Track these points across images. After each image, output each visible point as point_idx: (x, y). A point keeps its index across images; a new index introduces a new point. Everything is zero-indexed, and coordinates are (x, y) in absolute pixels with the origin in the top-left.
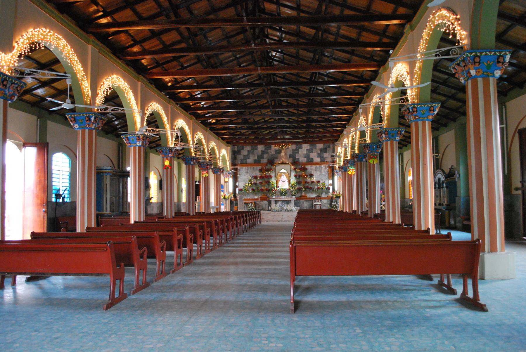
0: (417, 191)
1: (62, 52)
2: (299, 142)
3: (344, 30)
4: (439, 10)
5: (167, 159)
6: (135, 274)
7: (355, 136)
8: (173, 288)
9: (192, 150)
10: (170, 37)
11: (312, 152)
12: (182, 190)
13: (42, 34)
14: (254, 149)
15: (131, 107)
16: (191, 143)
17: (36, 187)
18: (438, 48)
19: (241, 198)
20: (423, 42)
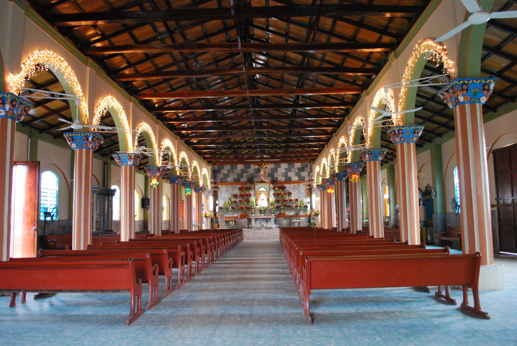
0: (404, 209)
1: (63, 74)
2: (278, 162)
3: (329, 56)
4: (424, 40)
5: (154, 177)
6: (149, 291)
7: (334, 156)
8: (185, 304)
9: (177, 169)
10: (160, 61)
11: (290, 171)
12: (163, 209)
13: (46, 57)
14: (233, 168)
15: (123, 128)
16: (176, 162)
17: (27, 205)
18: (421, 77)
19: (222, 216)
20: (408, 70)
